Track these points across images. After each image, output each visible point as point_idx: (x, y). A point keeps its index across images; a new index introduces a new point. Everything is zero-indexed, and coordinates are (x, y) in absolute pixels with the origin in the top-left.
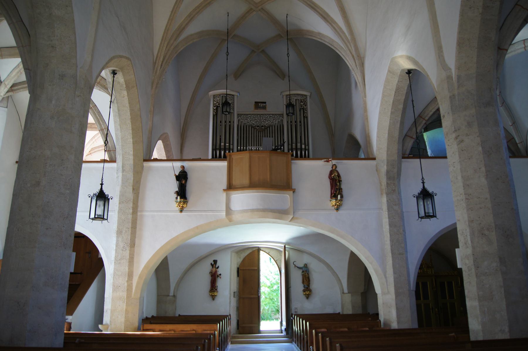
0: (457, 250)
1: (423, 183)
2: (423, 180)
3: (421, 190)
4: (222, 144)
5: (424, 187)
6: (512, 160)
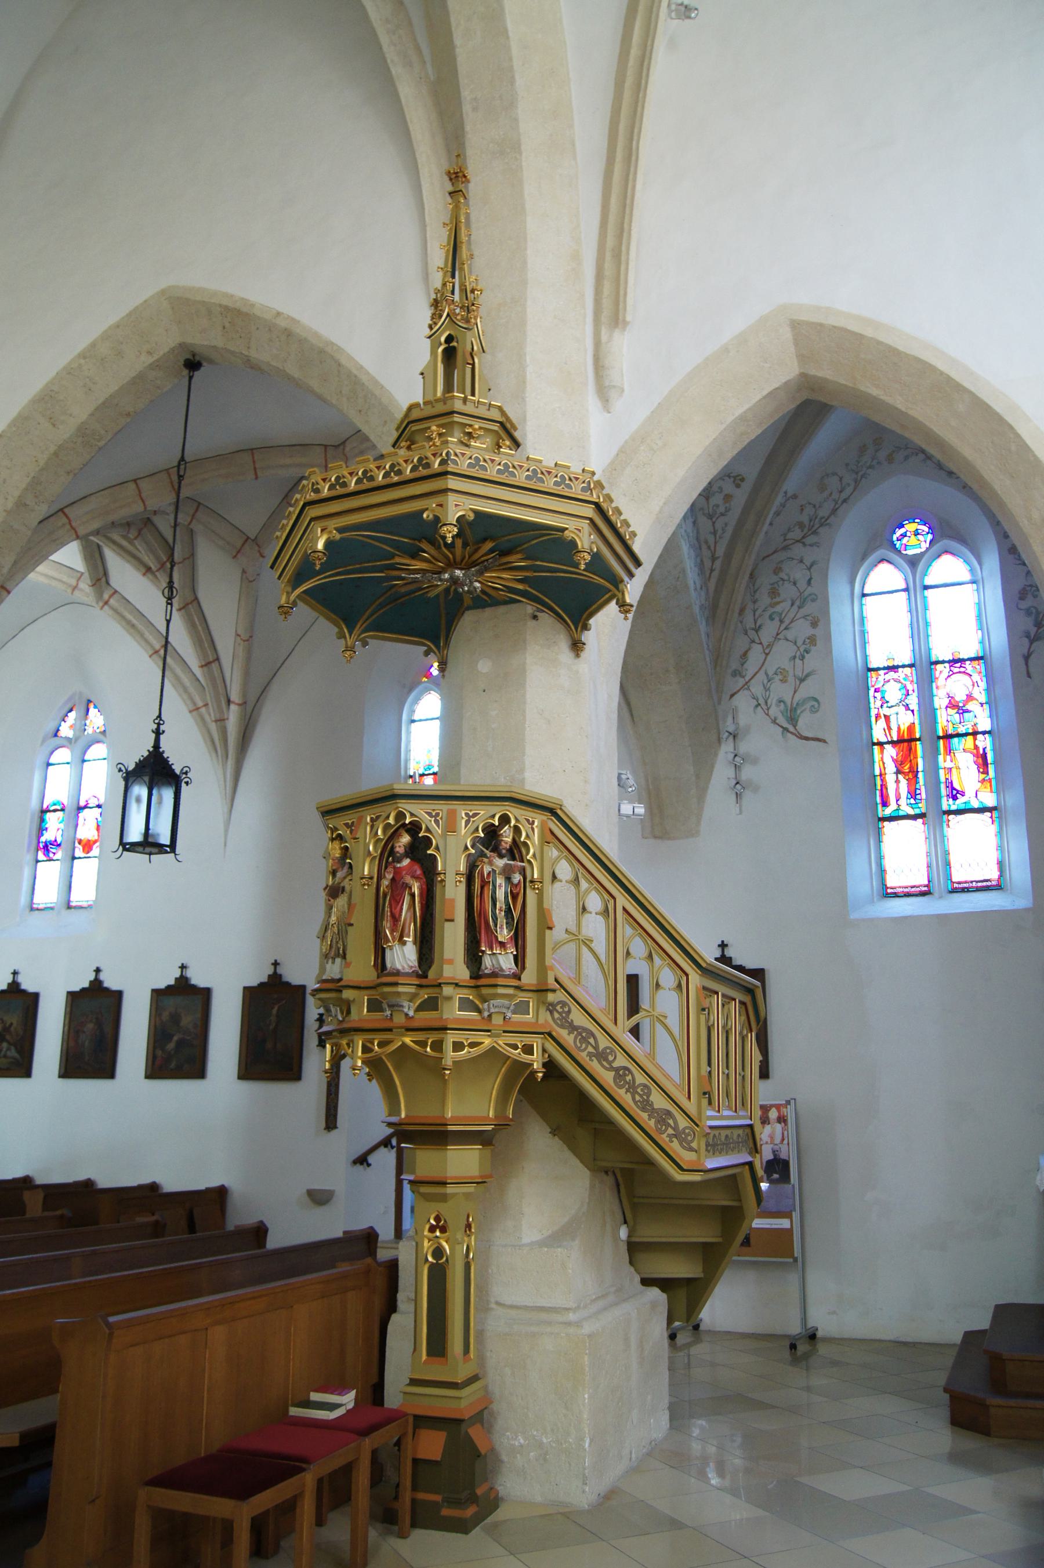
0: (761, 1059)
1: (158, 733)
2: (159, 724)
3: (146, 754)
4: (330, 466)
5: (157, 745)
6: (429, 977)
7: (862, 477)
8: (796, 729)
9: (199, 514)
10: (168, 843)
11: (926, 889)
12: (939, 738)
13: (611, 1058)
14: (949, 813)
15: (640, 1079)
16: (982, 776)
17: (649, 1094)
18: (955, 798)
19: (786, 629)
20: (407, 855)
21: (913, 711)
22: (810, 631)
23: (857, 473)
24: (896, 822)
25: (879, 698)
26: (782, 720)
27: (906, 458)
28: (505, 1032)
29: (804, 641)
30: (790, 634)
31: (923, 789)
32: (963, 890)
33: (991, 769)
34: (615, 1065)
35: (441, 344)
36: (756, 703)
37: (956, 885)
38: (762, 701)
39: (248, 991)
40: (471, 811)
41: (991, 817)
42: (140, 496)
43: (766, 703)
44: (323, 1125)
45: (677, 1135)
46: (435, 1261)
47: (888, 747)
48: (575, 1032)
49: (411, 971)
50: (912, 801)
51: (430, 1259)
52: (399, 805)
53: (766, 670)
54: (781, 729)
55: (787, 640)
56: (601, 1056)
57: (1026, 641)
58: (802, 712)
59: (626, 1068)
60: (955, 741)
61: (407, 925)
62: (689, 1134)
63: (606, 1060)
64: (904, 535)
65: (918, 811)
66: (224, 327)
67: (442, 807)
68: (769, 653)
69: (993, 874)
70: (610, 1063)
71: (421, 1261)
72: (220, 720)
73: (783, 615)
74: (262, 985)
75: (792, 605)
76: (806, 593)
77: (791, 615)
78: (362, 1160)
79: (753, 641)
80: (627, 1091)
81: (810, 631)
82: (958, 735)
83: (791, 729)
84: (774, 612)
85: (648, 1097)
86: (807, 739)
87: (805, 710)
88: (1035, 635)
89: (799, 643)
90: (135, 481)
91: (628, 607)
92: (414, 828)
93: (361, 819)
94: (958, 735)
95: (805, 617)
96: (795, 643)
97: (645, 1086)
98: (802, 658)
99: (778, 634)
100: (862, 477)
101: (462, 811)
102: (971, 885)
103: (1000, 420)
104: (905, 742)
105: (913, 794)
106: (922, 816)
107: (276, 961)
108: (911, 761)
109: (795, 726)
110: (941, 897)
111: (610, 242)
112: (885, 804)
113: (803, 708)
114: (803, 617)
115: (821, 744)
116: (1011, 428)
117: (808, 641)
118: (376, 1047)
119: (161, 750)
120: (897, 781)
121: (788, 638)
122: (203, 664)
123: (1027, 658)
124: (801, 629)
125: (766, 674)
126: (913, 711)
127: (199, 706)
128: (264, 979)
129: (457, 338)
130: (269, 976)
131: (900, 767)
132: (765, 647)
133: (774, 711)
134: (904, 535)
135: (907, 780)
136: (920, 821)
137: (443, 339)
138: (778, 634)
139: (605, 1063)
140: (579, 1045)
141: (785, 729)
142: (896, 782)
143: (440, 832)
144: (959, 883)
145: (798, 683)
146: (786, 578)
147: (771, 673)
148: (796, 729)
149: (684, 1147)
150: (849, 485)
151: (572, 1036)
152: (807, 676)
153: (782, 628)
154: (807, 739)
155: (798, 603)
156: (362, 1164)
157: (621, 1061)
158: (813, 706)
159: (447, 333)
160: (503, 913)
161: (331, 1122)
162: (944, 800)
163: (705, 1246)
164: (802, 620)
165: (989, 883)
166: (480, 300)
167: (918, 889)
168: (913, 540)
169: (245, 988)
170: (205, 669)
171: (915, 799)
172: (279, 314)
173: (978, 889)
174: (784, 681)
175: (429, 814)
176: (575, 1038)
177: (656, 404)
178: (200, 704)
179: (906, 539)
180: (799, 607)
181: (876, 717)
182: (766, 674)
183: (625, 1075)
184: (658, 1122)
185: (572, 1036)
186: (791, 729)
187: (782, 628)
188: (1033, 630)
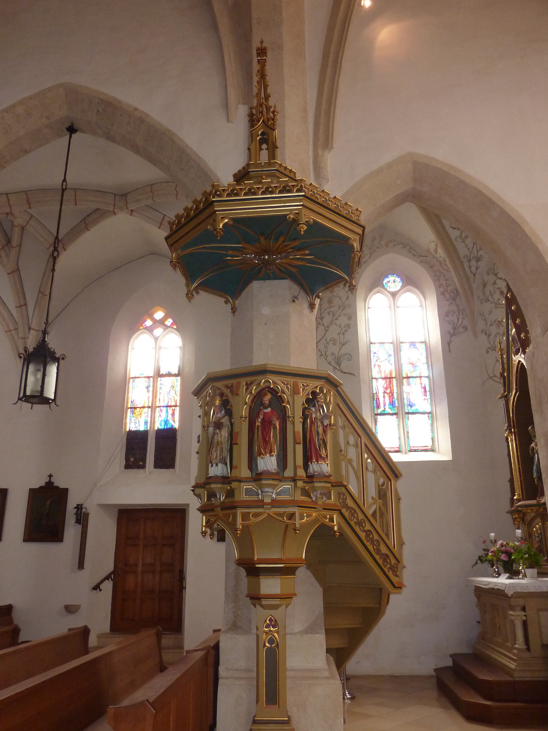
7: (373, 252)
8: (340, 368)
9: (31, 222)
10: (53, 398)
11: (398, 449)
12: (404, 378)
13: (364, 525)
14: (408, 413)
15: (376, 537)
16: (425, 397)
17: (379, 545)
18: (411, 406)
19: (336, 319)
20: (270, 405)
21: (391, 364)
22: (347, 322)
23: (371, 250)
24: (383, 416)
25: (376, 357)
26: (333, 363)
27: (394, 245)
28: (324, 509)
29: (345, 326)
30: (338, 322)
31: (396, 401)
32: (415, 451)
33: (428, 393)
34: (366, 529)
35: (258, 136)
36: (321, 354)
37: (412, 448)
38: (323, 353)
39: (32, 492)
40: (306, 383)
41: (428, 417)
42: (9, 203)
43: (326, 354)
44: (77, 566)
45: (391, 568)
46: (270, 646)
47: (380, 380)
48: (349, 510)
49: (276, 472)
50: (391, 407)
51: (267, 645)
52: (267, 377)
53: (326, 338)
54: (333, 368)
55: (337, 325)
56: (360, 524)
57: (449, 336)
58: (343, 360)
59: (370, 531)
60: (411, 379)
61: (273, 445)
62: (395, 568)
63: (362, 526)
64: (388, 282)
65: (394, 412)
66: (98, 111)
67: (291, 380)
68: (328, 330)
69: (429, 444)
70: (363, 528)
71: (261, 646)
72: (24, 338)
73: (335, 313)
74: (41, 488)
75: (339, 308)
76: (346, 304)
77: (338, 314)
78: (97, 587)
79: (320, 324)
80: (371, 543)
81: (347, 322)
82: (413, 377)
83: (338, 368)
84: (330, 311)
85: (379, 547)
86: (345, 373)
87: (344, 359)
88: (453, 333)
89: (342, 327)
90: (7, 194)
91: (353, 287)
92: (274, 392)
93: (239, 384)
94: (413, 377)
95: (345, 315)
96: (340, 327)
97: (378, 541)
98: (344, 334)
99: (332, 322)
100: (373, 252)
101: (301, 382)
102: (419, 448)
103: (514, 222)
104: (389, 379)
105: (392, 403)
106: (396, 414)
107: (51, 474)
108: (390, 388)
109: (339, 367)
110: (406, 453)
111: (324, 107)
112: (378, 407)
113: (343, 358)
114: (344, 315)
115: (352, 376)
116: (520, 227)
117: (346, 326)
118: (251, 517)
119: (47, 343)
120: (384, 397)
121: (337, 324)
122: (18, 305)
123: (449, 343)
124: (343, 320)
125: (326, 340)
126: (391, 364)
127: (12, 329)
128: (43, 484)
129: (267, 133)
130: (46, 482)
131: (385, 390)
132: (325, 327)
133: (330, 358)
134: (388, 282)
135: (389, 397)
136: (395, 416)
137: (260, 133)
138: (332, 322)
139: (361, 528)
140: (350, 517)
141: (335, 368)
142: (383, 397)
143: (289, 393)
144: (413, 447)
145: (341, 346)
146: (336, 295)
147: (328, 340)
148: (340, 368)
149: (394, 575)
150: (367, 255)
151: (348, 512)
152: (346, 343)
153: (334, 318)
154: (345, 373)
155: (341, 308)
156: (96, 590)
157: (368, 527)
158: (348, 357)
159: (262, 130)
160: (322, 441)
161: (81, 565)
162: (406, 407)
163: (350, 630)
164: (344, 316)
165: (427, 448)
166: (277, 117)
167: (394, 449)
168: (393, 284)
169: (30, 489)
170: (19, 309)
171: (392, 406)
172: (136, 109)
173: (422, 451)
174: (334, 344)
175: (284, 383)
176: (349, 514)
177: (345, 191)
178: (12, 328)
179: (390, 284)
180: (342, 310)
181: (374, 366)
182: (326, 340)
183: (370, 535)
184: (383, 561)
185: (348, 512)
186: (338, 368)
187: (334, 318)
188: (452, 331)
